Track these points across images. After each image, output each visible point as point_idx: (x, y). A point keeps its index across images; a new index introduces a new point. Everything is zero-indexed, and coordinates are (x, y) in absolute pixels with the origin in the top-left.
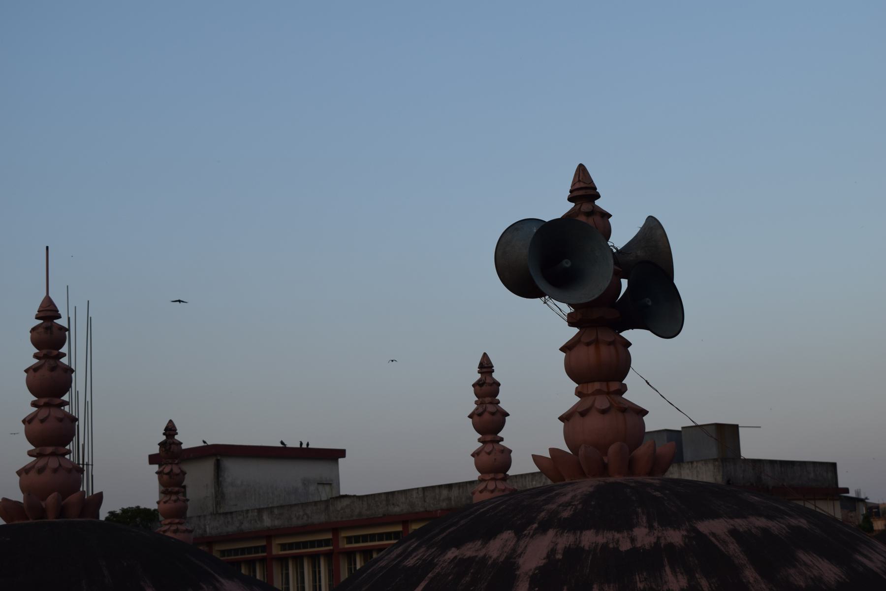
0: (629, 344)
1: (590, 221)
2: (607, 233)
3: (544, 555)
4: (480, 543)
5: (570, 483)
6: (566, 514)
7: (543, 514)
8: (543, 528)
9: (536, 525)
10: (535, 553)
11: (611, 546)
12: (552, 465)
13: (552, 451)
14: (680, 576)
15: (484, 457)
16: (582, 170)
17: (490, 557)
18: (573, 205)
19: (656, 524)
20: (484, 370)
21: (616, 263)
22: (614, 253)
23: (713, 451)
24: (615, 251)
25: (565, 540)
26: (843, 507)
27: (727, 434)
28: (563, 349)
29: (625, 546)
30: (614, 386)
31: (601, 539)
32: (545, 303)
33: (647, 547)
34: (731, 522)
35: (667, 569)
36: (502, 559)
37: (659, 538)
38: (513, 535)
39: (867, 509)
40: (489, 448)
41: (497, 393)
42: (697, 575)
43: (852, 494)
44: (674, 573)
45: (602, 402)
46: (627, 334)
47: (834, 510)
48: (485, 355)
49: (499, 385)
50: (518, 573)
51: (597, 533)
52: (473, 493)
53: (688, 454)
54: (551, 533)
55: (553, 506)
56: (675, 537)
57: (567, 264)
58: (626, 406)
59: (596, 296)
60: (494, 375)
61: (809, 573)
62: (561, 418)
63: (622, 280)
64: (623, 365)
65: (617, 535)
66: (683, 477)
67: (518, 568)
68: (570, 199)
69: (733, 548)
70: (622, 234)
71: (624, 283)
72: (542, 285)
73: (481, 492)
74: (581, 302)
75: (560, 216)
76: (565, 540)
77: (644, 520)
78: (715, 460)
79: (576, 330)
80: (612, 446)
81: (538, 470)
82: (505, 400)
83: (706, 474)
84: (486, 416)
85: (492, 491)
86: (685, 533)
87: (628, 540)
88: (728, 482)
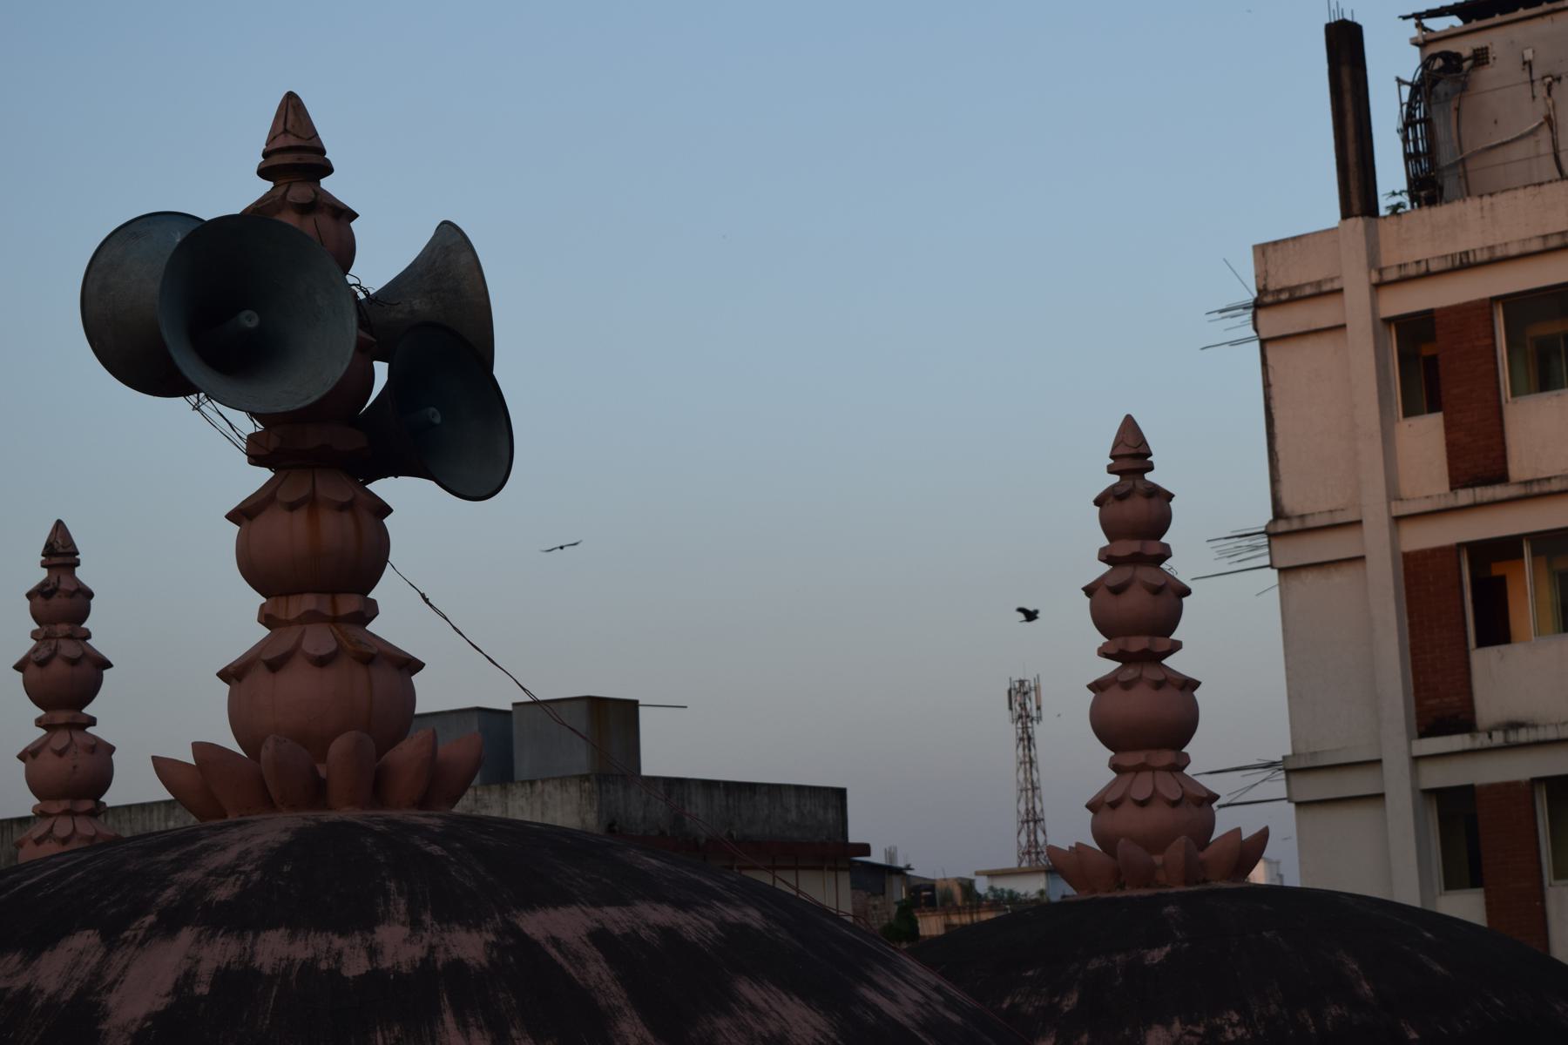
0: (387, 510)
1: (307, 225)
2: (345, 254)
3: (168, 985)
4: (17, 957)
5: (238, 824)
6: (223, 893)
7: (170, 892)
8: (169, 925)
9: (150, 919)
10: (147, 980)
11: (323, 966)
12: (199, 781)
13: (198, 748)
14: (475, 1035)
15: (48, 761)
16: (292, 106)
17: (41, 992)
18: (269, 185)
19: (427, 918)
20: (56, 560)
21: (363, 324)
22: (358, 302)
23: (580, 758)
24: (362, 296)
25: (220, 952)
26: (856, 885)
27: (613, 720)
28: (233, 516)
29: (356, 965)
30: (348, 604)
31: (301, 951)
32: (197, 408)
33: (405, 969)
34: (596, 913)
35: (448, 1018)
36: (68, 995)
37: (432, 949)
38: (98, 939)
39: (909, 891)
40: (61, 740)
41: (84, 613)
42: (514, 1033)
43: (877, 857)
44: (463, 1026)
45: (319, 640)
46: (382, 488)
47: (830, 893)
48: (59, 523)
49: (90, 595)
50: (104, 1027)
51: (292, 937)
52: (19, 845)
53: (524, 765)
54: (186, 936)
55: (194, 875)
56: (470, 946)
57: (249, 320)
58: (374, 651)
59: (315, 398)
60: (79, 572)
61: (758, 1028)
62: (224, 675)
63: (376, 364)
64: (369, 558)
65: (338, 942)
66: (510, 816)
67: (106, 1015)
68: (263, 173)
69: (597, 972)
70: (377, 263)
71: (381, 370)
72: (189, 364)
73: (38, 842)
74: (280, 409)
75: (237, 209)
76: (220, 952)
77: (402, 907)
78: (584, 778)
79: (264, 475)
80: (338, 741)
81: (168, 796)
82: (102, 630)
83: (563, 809)
84: (58, 667)
85: (65, 841)
86: (492, 938)
87: (363, 953)
88: (610, 829)
